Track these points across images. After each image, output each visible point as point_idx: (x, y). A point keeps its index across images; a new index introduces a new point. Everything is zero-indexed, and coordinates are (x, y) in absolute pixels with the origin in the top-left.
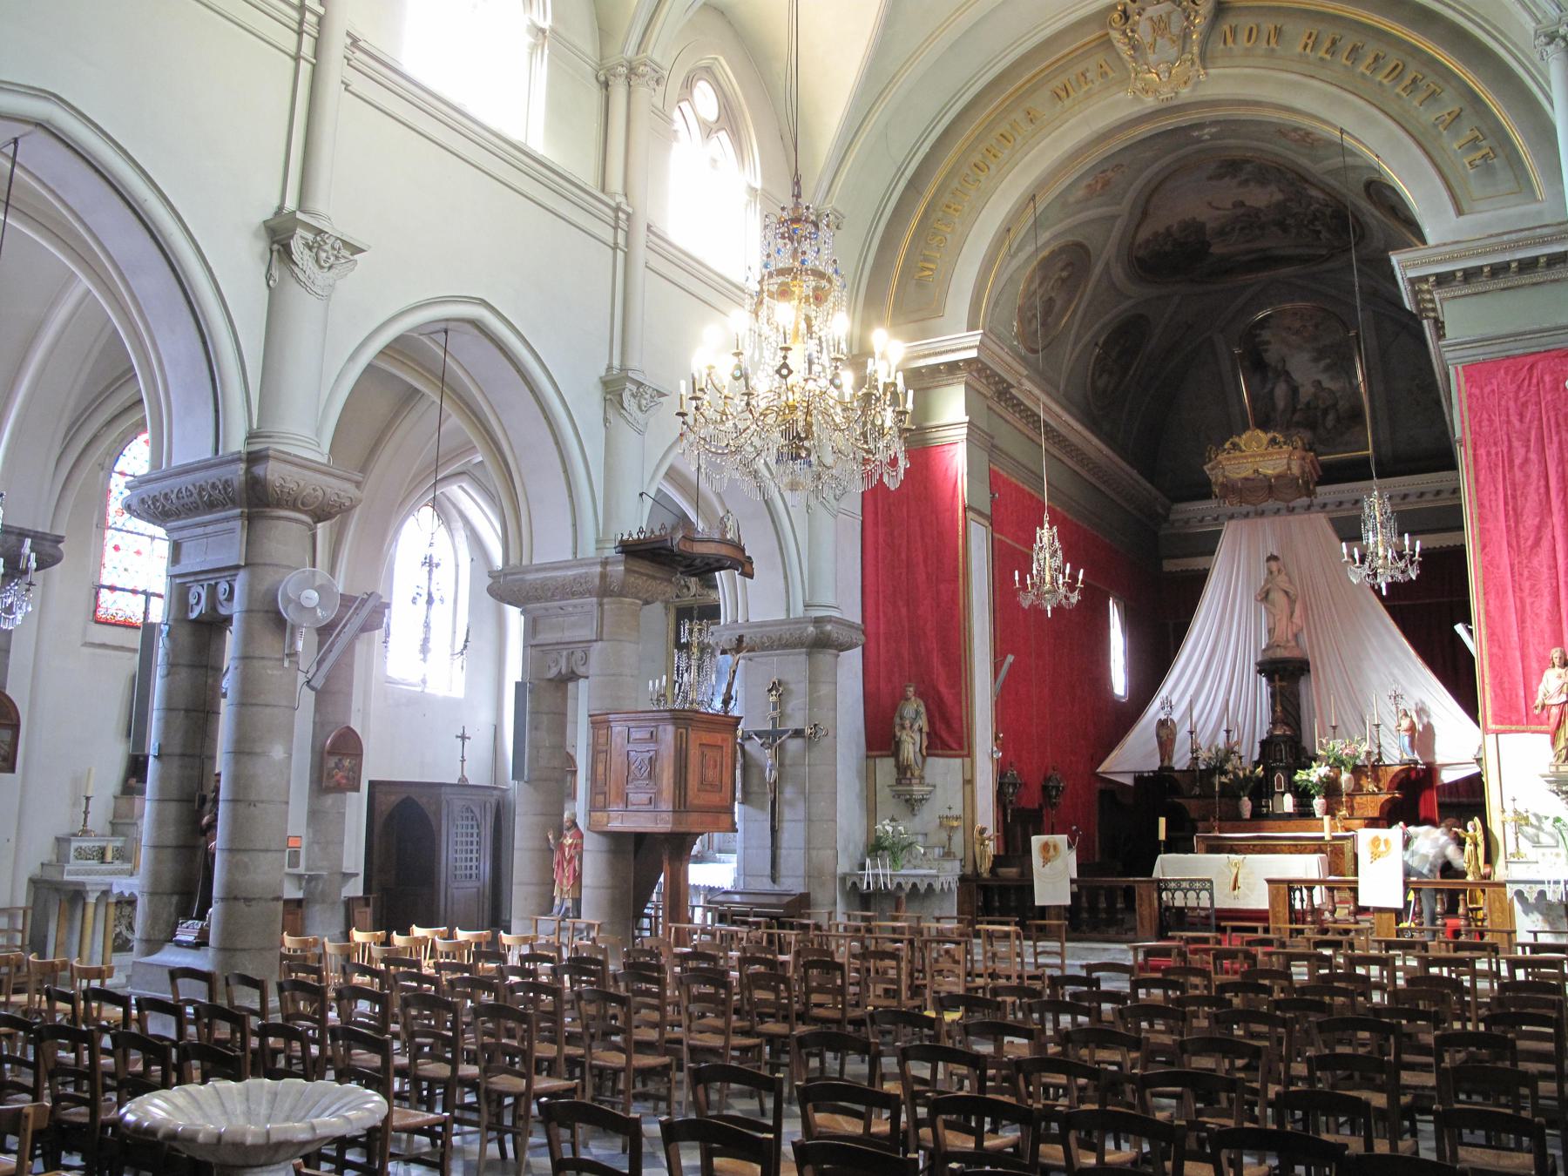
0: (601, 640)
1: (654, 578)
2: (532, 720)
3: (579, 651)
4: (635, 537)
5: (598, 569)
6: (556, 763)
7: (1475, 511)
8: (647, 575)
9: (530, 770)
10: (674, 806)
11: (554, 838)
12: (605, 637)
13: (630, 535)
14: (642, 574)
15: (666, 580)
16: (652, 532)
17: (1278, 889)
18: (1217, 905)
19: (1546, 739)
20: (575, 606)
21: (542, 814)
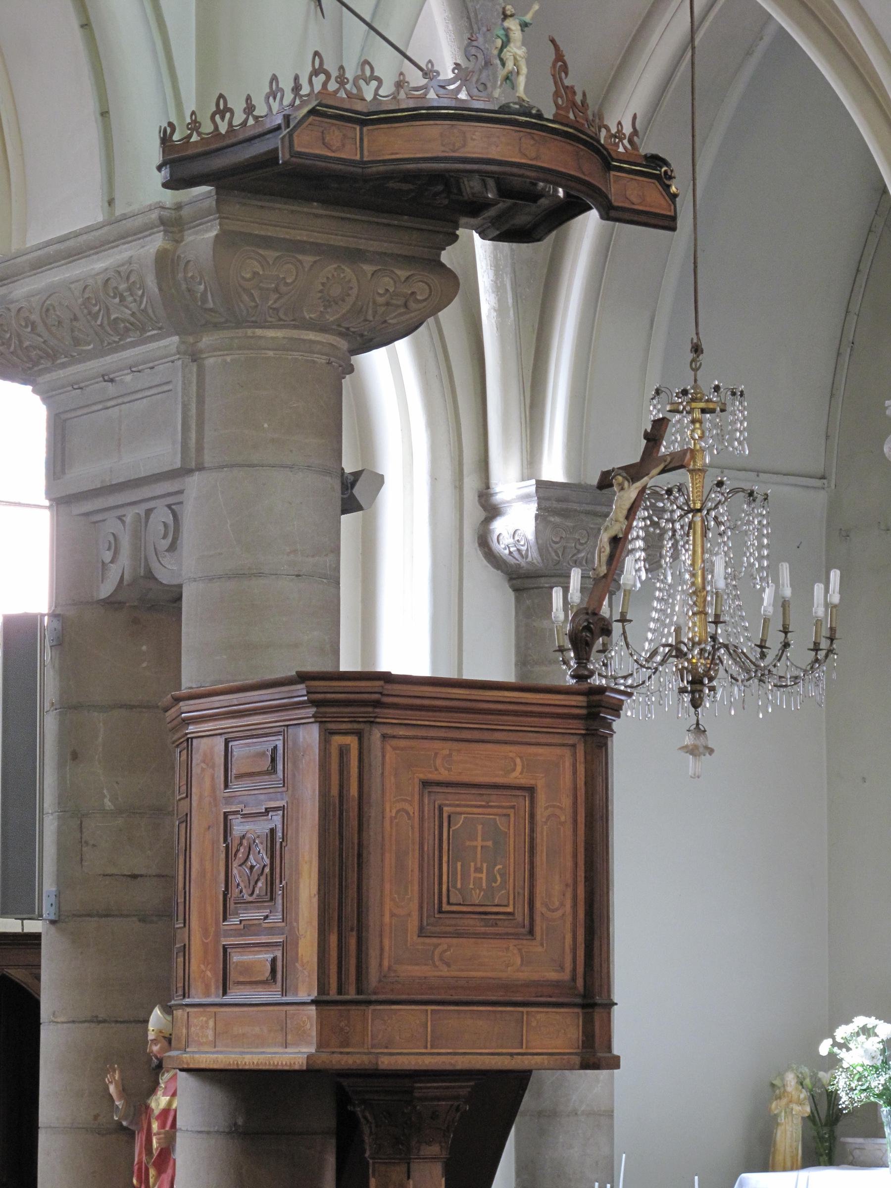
0: (200, 468)
1: (354, 256)
2: (66, 733)
3: (160, 504)
4: (207, 128)
5: (157, 242)
6: (138, 863)
7: (144, 351)
8: (317, 249)
9: (64, 881)
10: (322, 988)
11: (124, 1091)
12: (208, 459)
13: (250, 109)
14: (298, 247)
15: (409, 260)
16: (250, 109)
17: (359, 991)
18: (25, 931)
19: (614, 723)
20: (133, 368)
21: (95, 1020)
